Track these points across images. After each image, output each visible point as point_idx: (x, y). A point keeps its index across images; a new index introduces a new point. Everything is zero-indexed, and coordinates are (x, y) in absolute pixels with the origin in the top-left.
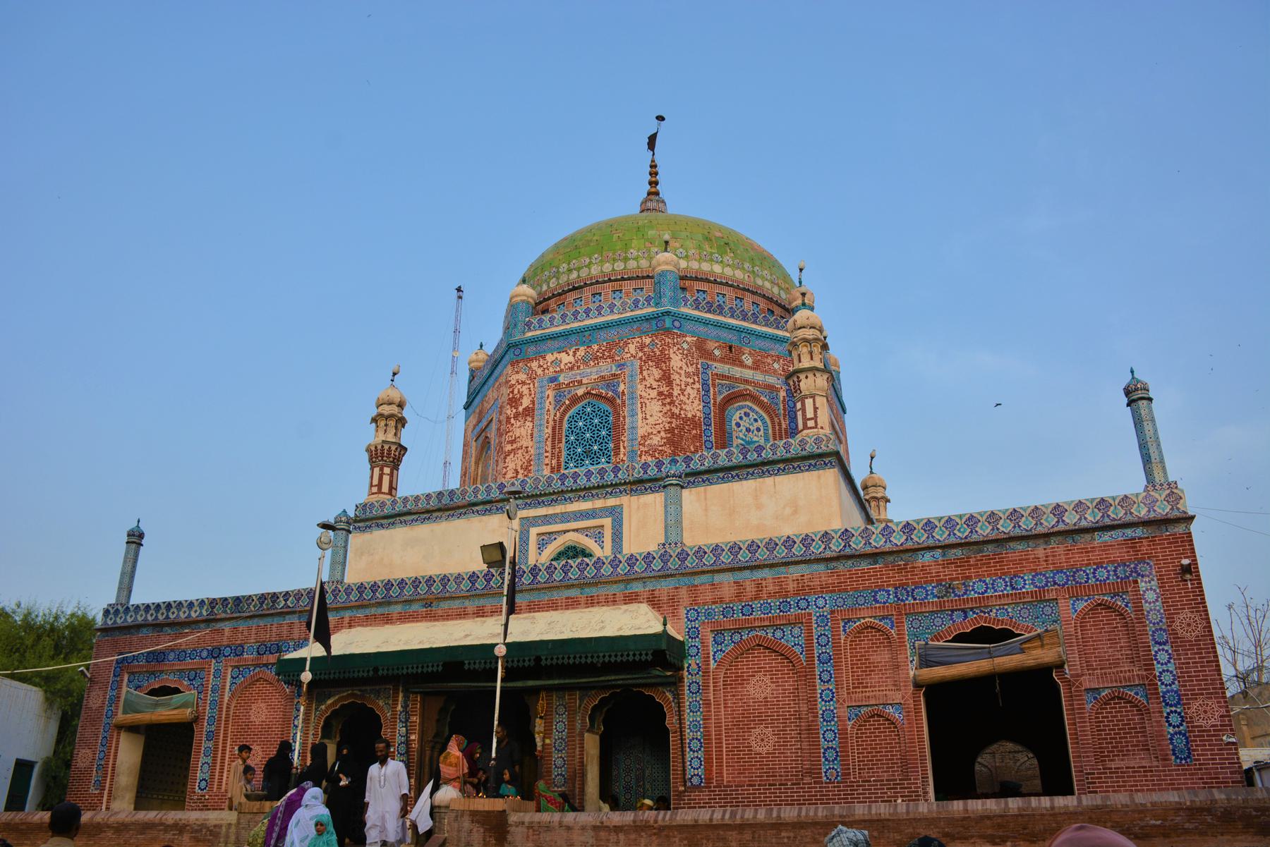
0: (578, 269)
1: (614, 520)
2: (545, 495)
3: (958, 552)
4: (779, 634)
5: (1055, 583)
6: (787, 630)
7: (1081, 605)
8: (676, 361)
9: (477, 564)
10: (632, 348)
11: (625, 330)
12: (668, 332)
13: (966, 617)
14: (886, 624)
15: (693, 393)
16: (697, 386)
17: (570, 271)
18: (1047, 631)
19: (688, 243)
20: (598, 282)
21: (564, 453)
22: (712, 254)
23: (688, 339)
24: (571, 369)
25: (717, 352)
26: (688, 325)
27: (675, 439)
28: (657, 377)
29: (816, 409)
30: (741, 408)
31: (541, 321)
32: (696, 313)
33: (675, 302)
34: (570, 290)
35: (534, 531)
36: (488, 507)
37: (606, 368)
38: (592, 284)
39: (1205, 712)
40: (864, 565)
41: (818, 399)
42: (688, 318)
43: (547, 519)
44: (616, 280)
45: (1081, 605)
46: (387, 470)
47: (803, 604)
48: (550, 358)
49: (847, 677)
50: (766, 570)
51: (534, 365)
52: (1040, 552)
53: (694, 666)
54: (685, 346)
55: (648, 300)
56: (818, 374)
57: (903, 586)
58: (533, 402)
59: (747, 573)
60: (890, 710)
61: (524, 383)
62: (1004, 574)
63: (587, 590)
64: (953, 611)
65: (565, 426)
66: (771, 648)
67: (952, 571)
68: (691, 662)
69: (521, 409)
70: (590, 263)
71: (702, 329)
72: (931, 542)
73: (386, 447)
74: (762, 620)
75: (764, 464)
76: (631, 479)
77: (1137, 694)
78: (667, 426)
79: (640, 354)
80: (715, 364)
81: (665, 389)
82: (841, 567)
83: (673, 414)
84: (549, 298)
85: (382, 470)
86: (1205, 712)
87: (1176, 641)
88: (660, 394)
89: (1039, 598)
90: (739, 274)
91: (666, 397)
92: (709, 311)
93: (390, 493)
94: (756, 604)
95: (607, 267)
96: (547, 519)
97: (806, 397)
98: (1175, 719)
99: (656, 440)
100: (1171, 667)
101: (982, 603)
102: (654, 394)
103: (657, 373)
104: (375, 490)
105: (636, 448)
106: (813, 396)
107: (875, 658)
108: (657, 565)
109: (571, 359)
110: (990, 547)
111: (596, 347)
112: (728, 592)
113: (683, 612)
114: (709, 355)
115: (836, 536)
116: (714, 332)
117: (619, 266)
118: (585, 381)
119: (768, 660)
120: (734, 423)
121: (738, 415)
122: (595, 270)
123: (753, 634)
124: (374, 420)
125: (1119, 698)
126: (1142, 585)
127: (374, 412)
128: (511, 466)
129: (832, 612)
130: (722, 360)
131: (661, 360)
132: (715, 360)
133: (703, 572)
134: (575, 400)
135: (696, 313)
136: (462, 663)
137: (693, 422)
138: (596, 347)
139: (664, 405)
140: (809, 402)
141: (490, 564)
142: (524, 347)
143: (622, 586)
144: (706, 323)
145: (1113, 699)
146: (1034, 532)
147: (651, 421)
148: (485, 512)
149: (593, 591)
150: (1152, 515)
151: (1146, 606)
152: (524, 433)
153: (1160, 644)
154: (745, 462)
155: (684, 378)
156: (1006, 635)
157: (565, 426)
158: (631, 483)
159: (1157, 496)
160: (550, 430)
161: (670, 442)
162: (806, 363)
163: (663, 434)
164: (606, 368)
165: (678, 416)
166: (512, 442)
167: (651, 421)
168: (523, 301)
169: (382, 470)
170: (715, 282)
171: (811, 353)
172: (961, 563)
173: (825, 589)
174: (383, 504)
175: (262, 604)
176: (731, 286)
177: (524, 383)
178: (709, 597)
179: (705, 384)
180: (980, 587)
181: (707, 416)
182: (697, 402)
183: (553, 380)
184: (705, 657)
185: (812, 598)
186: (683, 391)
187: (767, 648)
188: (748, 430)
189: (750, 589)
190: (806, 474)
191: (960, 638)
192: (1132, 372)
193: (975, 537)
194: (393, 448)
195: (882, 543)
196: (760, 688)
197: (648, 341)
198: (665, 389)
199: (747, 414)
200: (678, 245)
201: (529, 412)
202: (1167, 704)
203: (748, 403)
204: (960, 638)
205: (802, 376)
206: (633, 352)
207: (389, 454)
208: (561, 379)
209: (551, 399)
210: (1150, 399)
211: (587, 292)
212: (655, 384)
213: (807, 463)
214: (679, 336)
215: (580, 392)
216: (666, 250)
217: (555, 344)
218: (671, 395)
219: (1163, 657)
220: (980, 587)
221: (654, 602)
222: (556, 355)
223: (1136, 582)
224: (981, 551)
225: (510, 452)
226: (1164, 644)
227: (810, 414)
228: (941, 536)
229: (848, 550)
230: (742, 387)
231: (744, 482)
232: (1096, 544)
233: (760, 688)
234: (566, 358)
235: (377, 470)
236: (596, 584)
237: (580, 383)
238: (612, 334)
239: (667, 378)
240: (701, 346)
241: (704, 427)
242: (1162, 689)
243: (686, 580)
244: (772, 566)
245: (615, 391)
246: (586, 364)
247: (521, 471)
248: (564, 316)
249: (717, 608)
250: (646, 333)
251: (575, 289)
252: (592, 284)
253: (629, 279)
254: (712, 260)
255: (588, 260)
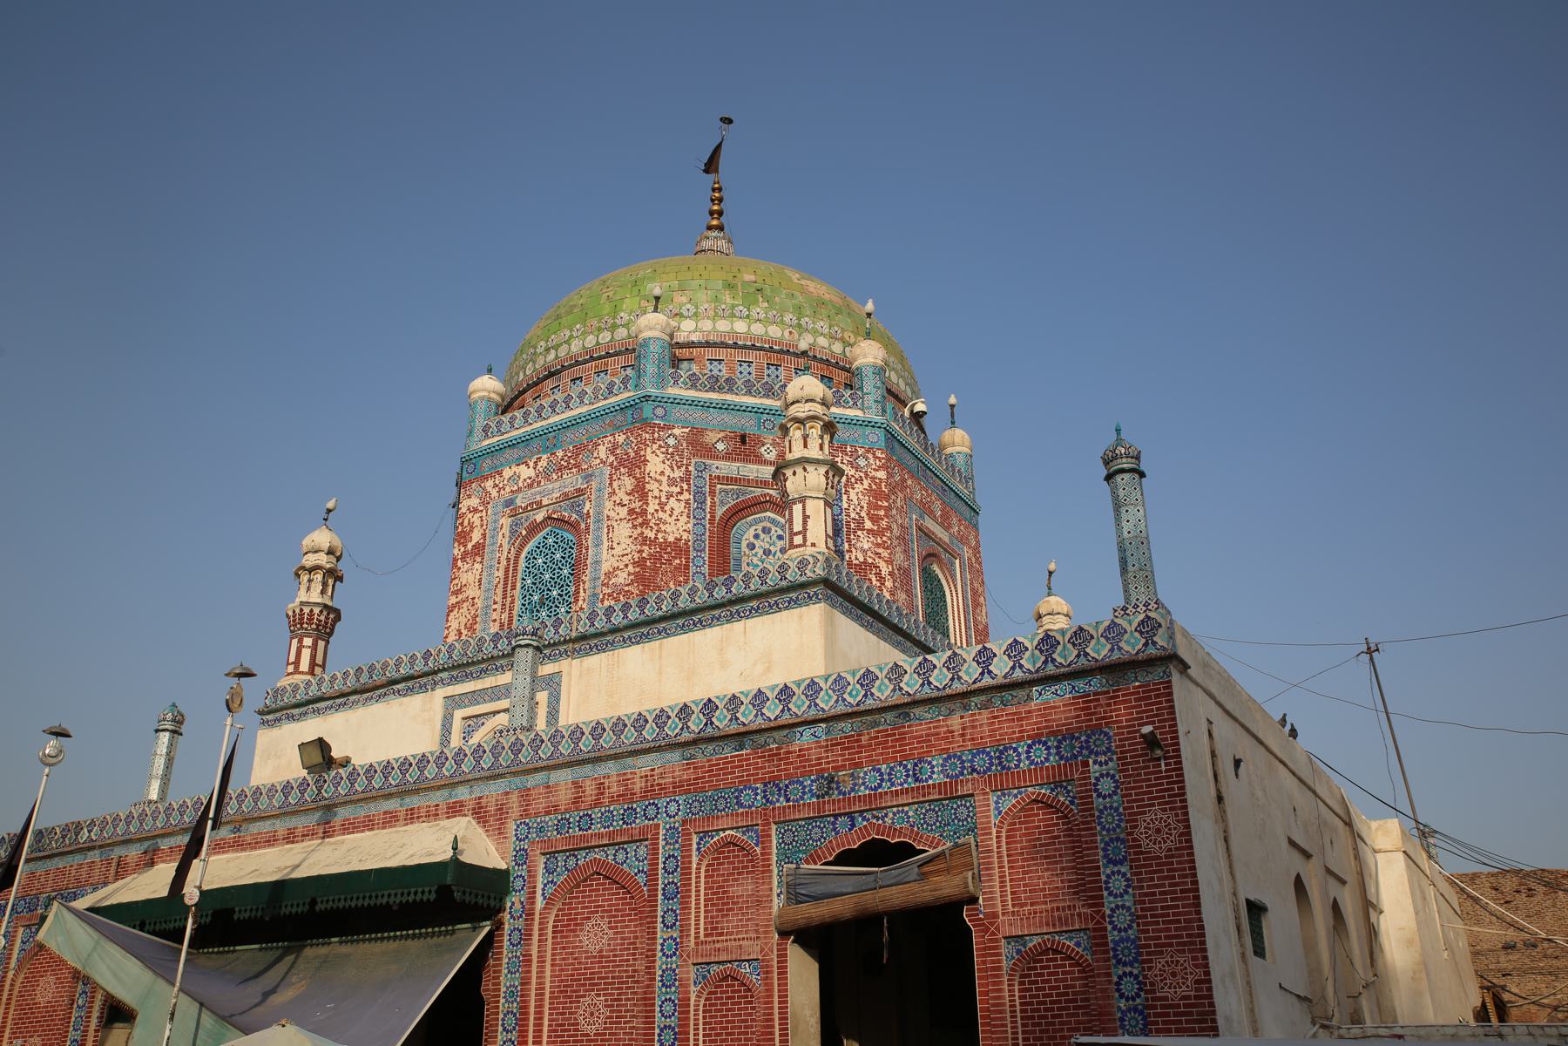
0: (556, 348)
1: (551, 694)
2: (473, 663)
3: (846, 726)
4: (621, 857)
5: (974, 770)
6: (631, 848)
7: (1008, 802)
8: (655, 463)
9: (295, 770)
10: (602, 451)
11: (595, 427)
12: (646, 424)
13: (853, 825)
14: (747, 838)
15: (679, 507)
16: (686, 496)
17: (548, 350)
18: (956, 845)
19: (701, 296)
20: (577, 363)
21: (518, 604)
22: (733, 306)
23: (677, 431)
24: (530, 486)
25: (721, 446)
26: (677, 412)
27: (646, 575)
28: (629, 488)
29: (806, 518)
30: (756, 522)
31: (500, 423)
32: (692, 394)
33: (661, 382)
34: (546, 377)
35: (459, 714)
36: (410, 684)
37: (571, 481)
38: (571, 366)
39: (1174, 974)
40: (728, 752)
41: (809, 503)
42: (676, 402)
43: (475, 697)
44: (600, 358)
45: (1008, 802)
46: (308, 641)
47: (651, 811)
48: (507, 473)
49: (698, 920)
50: (611, 764)
51: (489, 484)
52: (955, 722)
53: (518, 906)
54: (671, 441)
55: (625, 381)
56: (810, 468)
57: (774, 780)
58: (484, 535)
59: (588, 768)
60: (746, 969)
61: (475, 510)
62: (905, 757)
63: (407, 800)
64: (836, 816)
65: (522, 564)
66: (612, 876)
67: (837, 757)
68: (514, 901)
69: (469, 546)
70: (571, 337)
71: (697, 416)
72: (813, 713)
73: (307, 610)
74: (600, 836)
75: (732, 602)
76: (574, 634)
77: (1078, 944)
78: (637, 556)
79: (612, 458)
80: (717, 463)
81: (637, 505)
82: (704, 755)
83: (645, 539)
84: (525, 391)
85: (300, 641)
86: (1174, 974)
87: (1137, 858)
88: (631, 512)
89: (950, 794)
90: (775, 332)
91: (638, 517)
92: (712, 389)
93: (311, 672)
94: (596, 813)
95: (590, 341)
96: (475, 697)
97: (794, 501)
98: (1129, 986)
99: (622, 578)
100: (1128, 900)
101: (874, 803)
102: (623, 512)
103: (629, 483)
104: (291, 669)
105: (598, 590)
106: (803, 500)
107: (736, 890)
108: (487, 762)
109: (531, 472)
110: (889, 716)
111: (560, 454)
112: (564, 796)
113: (511, 826)
114: (710, 452)
115: (697, 711)
116: (715, 417)
117: (605, 337)
118: (545, 502)
119: (607, 896)
120: (744, 544)
121: (752, 532)
122: (576, 347)
123: (592, 856)
124: (1109, 478)
125: (1056, 951)
126: (1094, 769)
127: (1105, 473)
128: (454, 625)
129: (684, 822)
130: (728, 457)
131: (634, 464)
132: (717, 458)
133: (536, 770)
134: (534, 529)
135: (692, 394)
136: (233, 911)
137: (679, 548)
138: (560, 454)
139: (634, 527)
140: (797, 508)
141: (310, 768)
142: (479, 462)
143: (445, 792)
144: (706, 406)
145: (1046, 952)
146: (948, 691)
147: (618, 550)
148: (410, 691)
149: (414, 801)
150: (1116, 656)
151: (1098, 802)
152: (471, 580)
153: (1115, 863)
154: (711, 602)
155: (665, 487)
156: (905, 851)
157: (522, 564)
158: (574, 641)
159: (1125, 624)
160: (501, 574)
161: (639, 578)
162: (798, 452)
163: (630, 568)
164: (571, 481)
165: (654, 542)
166: (456, 593)
167: (618, 550)
168: (482, 398)
169: (300, 641)
170: (735, 346)
171: (805, 437)
172: (850, 743)
173: (679, 788)
174: (296, 688)
175: (64, 837)
176: (761, 349)
177: (475, 510)
178: (542, 805)
179: (699, 493)
180: (872, 779)
181: (699, 538)
182: (684, 519)
183: (509, 503)
184: (536, 891)
185: (662, 803)
186: (662, 505)
187: (606, 877)
188: (767, 552)
189: (590, 789)
190: (785, 613)
191: (845, 858)
192: (1118, 431)
193: (870, 703)
194: (317, 610)
195: (751, 717)
196: (595, 937)
197: (621, 439)
198: (637, 505)
199: (766, 531)
200: (684, 299)
201: (479, 549)
202: (1119, 962)
203: (768, 514)
204: (845, 858)
205: (789, 472)
206: (603, 456)
207: (310, 619)
208: (519, 502)
209: (506, 530)
210: (1142, 475)
211: (566, 377)
212: (626, 499)
213: (787, 597)
214: (662, 428)
215: (540, 517)
216: (656, 310)
217: (515, 453)
218: (644, 512)
219: (1118, 884)
220: (872, 779)
221: (480, 814)
222: (514, 468)
223: (1086, 764)
224: (876, 724)
225: (454, 606)
226: (1121, 862)
227: (797, 527)
228: (826, 703)
229: (709, 729)
230: (758, 492)
231: (708, 630)
232: (1033, 705)
233: (595, 937)
234: (526, 472)
235: (295, 642)
236: (416, 791)
237: (540, 506)
238: (579, 435)
239: (640, 491)
240: (697, 444)
241: (692, 554)
242: (1113, 935)
243: (517, 780)
244: (616, 757)
245: (580, 513)
246: (548, 478)
247: (465, 632)
248: (526, 415)
249: (551, 820)
250: (618, 428)
251: (551, 375)
252: (571, 366)
253: (616, 354)
254: (733, 315)
255: (568, 334)
